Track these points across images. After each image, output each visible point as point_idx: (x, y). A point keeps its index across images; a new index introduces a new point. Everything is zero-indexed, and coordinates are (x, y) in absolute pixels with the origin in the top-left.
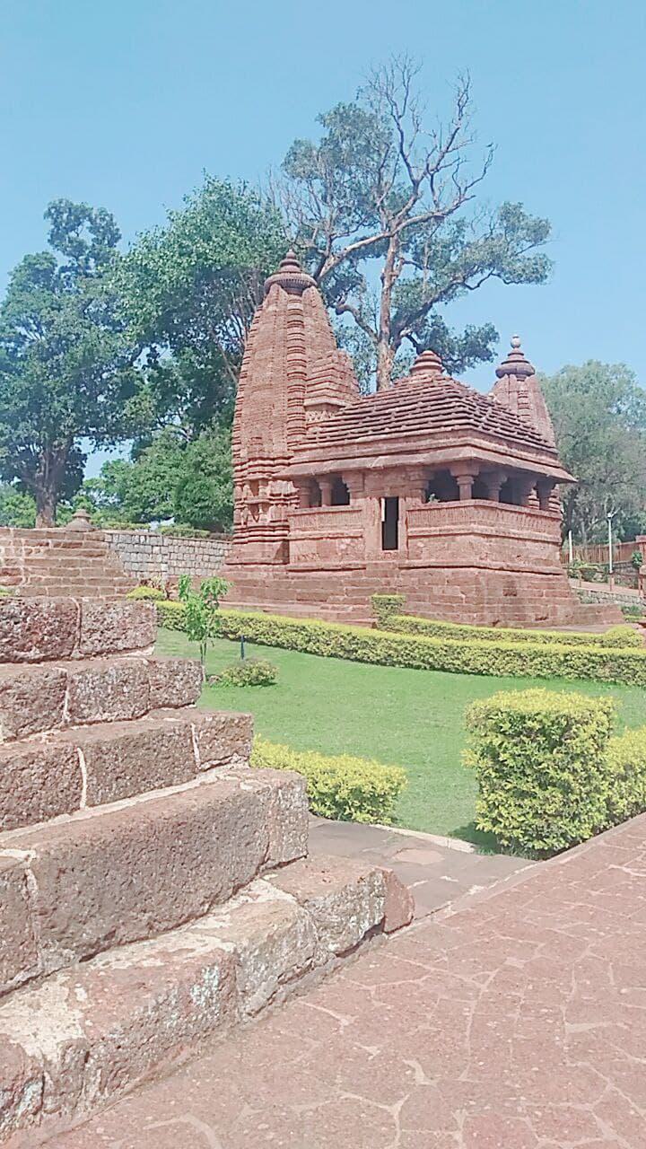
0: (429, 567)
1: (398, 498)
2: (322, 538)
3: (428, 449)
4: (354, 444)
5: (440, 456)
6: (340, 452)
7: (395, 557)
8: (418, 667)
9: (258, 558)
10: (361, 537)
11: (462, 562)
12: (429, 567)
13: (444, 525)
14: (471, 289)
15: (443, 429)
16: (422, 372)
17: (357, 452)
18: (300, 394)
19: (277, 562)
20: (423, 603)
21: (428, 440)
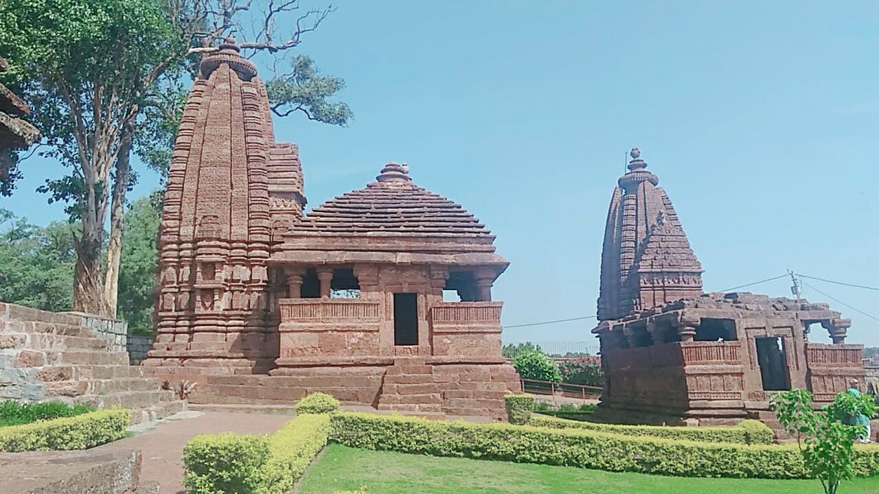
0: (460, 363)
1: (415, 295)
2: (326, 331)
3: (452, 252)
4: (366, 237)
6: (347, 243)
7: (417, 352)
8: (737, 476)
9: (214, 350)
11: (495, 359)
12: (460, 363)
13: (473, 323)
14: (280, 116)
15: (468, 235)
16: (396, 179)
17: (372, 245)
18: (265, 179)
19: (235, 355)
20: (466, 399)
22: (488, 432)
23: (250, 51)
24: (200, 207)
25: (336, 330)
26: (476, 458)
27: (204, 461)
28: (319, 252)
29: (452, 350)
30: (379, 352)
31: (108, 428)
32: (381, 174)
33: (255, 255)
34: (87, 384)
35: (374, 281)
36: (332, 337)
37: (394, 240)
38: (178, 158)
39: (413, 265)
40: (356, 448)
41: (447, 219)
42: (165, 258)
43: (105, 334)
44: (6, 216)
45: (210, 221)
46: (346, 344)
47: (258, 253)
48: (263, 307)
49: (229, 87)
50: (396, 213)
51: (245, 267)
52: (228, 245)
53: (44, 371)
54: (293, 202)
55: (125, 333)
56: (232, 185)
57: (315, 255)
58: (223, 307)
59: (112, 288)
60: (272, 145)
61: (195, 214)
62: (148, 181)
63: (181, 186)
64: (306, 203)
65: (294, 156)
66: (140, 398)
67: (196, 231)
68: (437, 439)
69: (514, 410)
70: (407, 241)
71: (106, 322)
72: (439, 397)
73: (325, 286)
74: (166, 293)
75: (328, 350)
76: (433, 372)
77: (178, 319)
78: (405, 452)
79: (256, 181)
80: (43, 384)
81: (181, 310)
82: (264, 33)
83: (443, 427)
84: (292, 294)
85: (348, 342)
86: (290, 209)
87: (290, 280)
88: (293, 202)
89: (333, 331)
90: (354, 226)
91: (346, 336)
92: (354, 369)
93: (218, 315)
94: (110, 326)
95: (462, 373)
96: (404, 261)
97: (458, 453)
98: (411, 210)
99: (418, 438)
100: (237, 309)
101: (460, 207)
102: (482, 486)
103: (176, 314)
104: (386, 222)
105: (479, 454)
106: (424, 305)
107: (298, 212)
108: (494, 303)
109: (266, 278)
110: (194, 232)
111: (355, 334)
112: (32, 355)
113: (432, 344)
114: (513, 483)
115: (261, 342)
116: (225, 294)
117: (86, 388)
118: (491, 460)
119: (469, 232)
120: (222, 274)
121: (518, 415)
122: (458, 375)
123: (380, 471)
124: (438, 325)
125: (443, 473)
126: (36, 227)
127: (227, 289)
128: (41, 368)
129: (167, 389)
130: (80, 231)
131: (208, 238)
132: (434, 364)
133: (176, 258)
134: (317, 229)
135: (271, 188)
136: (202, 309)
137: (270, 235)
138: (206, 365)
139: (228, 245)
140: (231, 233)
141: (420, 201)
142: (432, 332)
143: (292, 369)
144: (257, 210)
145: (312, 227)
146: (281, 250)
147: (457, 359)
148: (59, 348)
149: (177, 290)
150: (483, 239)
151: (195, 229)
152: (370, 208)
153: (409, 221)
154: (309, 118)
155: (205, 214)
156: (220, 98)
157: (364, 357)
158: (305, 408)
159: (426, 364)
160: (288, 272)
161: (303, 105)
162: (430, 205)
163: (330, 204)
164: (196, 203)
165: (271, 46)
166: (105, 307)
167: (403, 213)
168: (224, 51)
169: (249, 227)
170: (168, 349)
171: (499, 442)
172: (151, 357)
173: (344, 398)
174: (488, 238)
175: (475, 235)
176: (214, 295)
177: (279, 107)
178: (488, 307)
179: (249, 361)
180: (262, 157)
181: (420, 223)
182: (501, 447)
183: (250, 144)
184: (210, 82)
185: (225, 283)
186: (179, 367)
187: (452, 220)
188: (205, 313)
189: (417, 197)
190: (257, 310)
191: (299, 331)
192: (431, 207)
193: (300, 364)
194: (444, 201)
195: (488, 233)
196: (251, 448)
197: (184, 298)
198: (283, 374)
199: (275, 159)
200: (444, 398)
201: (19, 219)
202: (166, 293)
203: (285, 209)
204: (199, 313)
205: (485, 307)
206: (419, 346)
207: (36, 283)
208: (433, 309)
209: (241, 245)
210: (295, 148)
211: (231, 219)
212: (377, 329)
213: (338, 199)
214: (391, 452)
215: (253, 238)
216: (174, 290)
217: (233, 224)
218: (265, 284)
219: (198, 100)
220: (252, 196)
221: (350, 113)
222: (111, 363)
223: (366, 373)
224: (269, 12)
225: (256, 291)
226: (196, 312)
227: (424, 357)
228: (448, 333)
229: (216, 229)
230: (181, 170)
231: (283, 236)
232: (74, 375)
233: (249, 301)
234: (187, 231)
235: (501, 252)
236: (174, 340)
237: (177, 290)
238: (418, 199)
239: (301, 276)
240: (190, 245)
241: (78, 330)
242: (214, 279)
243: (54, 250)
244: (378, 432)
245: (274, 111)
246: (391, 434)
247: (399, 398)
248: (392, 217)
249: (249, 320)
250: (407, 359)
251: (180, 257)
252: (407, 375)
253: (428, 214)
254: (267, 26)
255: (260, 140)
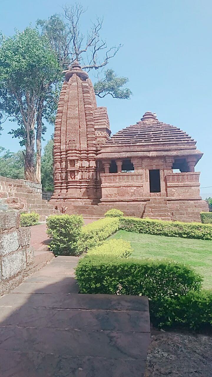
0: (180, 200)
1: (159, 170)
3: (176, 150)
5: (179, 153)
6: (128, 149)
10: (142, 187)
12: (180, 200)
13: (186, 182)
15: (183, 142)
17: (139, 149)
18: (93, 123)
19: (84, 198)
20: (183, 216)
21: (175, 146)
22: (190, 226)
23: (87, 70)
24: (68, 137)
25: (124, 186)
26: (185, 238)
27: (54, 224)
28: (116, 153)
29: (176, 194)
30: (143, 196)
31: (30, 220)
32: (143, 117)
33: (90, 156)
34: (24, 205)
35: (140, 165)
36: (123, 189)
37: (149, 146)
38: (58, 117)
39: (157, 157)
40: (130, 232)
41: (173, 135)
42: (55, 159)
43: (33, 188)
44: (2, 149)
45: (72, 142)
46: (129, 192)
47: (91, 155)
48: (95, 178)
49: (77, 84)
50: (149, 134)
51: (86, 162)
52: (79, 152)
53: (8, 199)
54: (105, 132)
55: (41, 188)
56: (80, 127)
57: (115, 154)
58: (79, 178)
59: (38, 173)
60: (95, 108)
61: (66, 140)
62: (50, 129)
63: (60, 128)
64: (111, 133)
65: (105, 112)
66: (45, 211)
67: (67, 147)
68: (166, 229)
69: (204, 219)
70: (154, 146)
71: (33, 183)
72: (170, 214)
73: (119, 168)
74: (57, 173)
75: (122, 195)
76: (167, 204)
77: (62, 183)
78: (152, 234)
79: (89, 124)
80: (7, 204)
81: (63, 180)
82: (93, 61)
83: (169, 224)
84: (105, 172)
85: (130, 191)
86: (104, 135)
87: (105, 166)
88: (105, 132)
89: (123, 187)
90: (131, 141)
91: (129, 189)
92: (133, 203)
93: (77, 181)
94: (35, 185)
95: (181, 204)
96: (153, 155)
97: (176, 235)
98: (156, 132)
99: (158, 228)
100: (84, 179)
101: (179, 129)
102: (184, 247)
103: (61, 181)
104: (145, 138)
105: (186, 236)
106: (163, 175)
107: (107, 137)
108: (196, 173)
109: (95, 166)
110: (66, 147)
111: (133, 188)
112: (3, 193)
113: (167, 192)
114: (200, 247)
115: (94, 191)
116: (79, 173)
117: (23, 206)
118: (191, 239)
119: (183, 141)
120: (78, 165)
121: (206, 221)
122: (179, 205)
123: (139, 240)
124: (169, 183)
125: (167, 242)
126: (13, 153)
127: (80, 170)
128: (6, 199)
129: (57, 209)
130: (25, 150)
131: (71, 150)
132: (168, 200)
133: (60, 158)
134: (115, 143)
135: (96, 127)
136: (71, 179)
137: (96, 147)
138: (73, 201)
139: (79, 152)
140: (80, 147)
141: (161, 128)
142: (167, 187)
143: (107, 203)
144: (90, 137)
145: (113, 142)
146: (101, 153)
147: (179, 198)
148: (14, 192)
149: (61, 172)
150: (190, 143)
151: (66, 146)
152: (138, 133)
153: (156, 137)
154: (113, 97)
155: (70, 140)
156: (73, 89)
157: (136, 198)
158: (109, 215)
159: (164, 200)
160: (104, 162)
161: (110, 92)
162: (165, 129)
163: (120, 132)
164: (66, 135)
165: (96, 66)
166: (36, 181)
167: (152, 134)
168: (75, 68)
169: (87, 144)
170: (59, 195)
171: (195, 231)
172: (53, 199)
173: (129, 215)
174: (193, 143)
175: (186, 142)
176: (75, 173)
177: (101, 93)
178: (193, 175)
179: (90, 200)
180: (91, 113)
181: (160, 138)
182: (196, 233)
183: (86, 108)
184: (69, 83)
185: (79, 168)
186: (63, 202)
187: (175, 135)
188: (71, 181)
189: (159, 126)
190: (93, 179)
191: (109, 187)
192: (166, 130)
193: (110, 201)
194: (172, 127)
195: (190, 138)
196: (73, 219)
197: (64, 175)
198: (103, 205)
199: (97, 114)
200: (173, 215)
201: (7, 151)
202: (57, 173)
203: (102, 135)
204: (70, 181)
205: (191, 175)
206: (161, 193)
207: (14, 175)
208: (167, 176)
209: (85, 152)
210: (105, 109)
211: (80, 141)
212: (142, 186)
213: (124, 130)
214: (146, 234)
215: (89, 149)
216: (60, 172)
217: (81, 143)
218: (95, 168)
219: (65, 91)
220: (88, 131)
221: (131, 92)
222: (34, 198)
223: (138, 205)
224: (94, 51)
225: (91, 171)
226: (69, 180)
227: (164, 197)
228: (174, 187)
229: (74, 146)
230: (60, 122)
231: (101, 147)
232: (19, 202)
233: (89, 175)
234: (63, 147)
235: (199, 149)
236: (61, 192)
237: (61, 172)
238: (160, 127)
239: (109, 164)
240: (65, 153)
241: (22, 186)
242: (75, 166)
243: (20, 162)
244: (140, 226)
245: (98, 96)
246: (146, 226)
247: (152, 215)
248: (148, 136)
249: (89, 183)
250: (155, 198)
251: (61, 158)
252: (155, 205)
253: (164, 134)
254: (94, 57)
255: (90, 106)
